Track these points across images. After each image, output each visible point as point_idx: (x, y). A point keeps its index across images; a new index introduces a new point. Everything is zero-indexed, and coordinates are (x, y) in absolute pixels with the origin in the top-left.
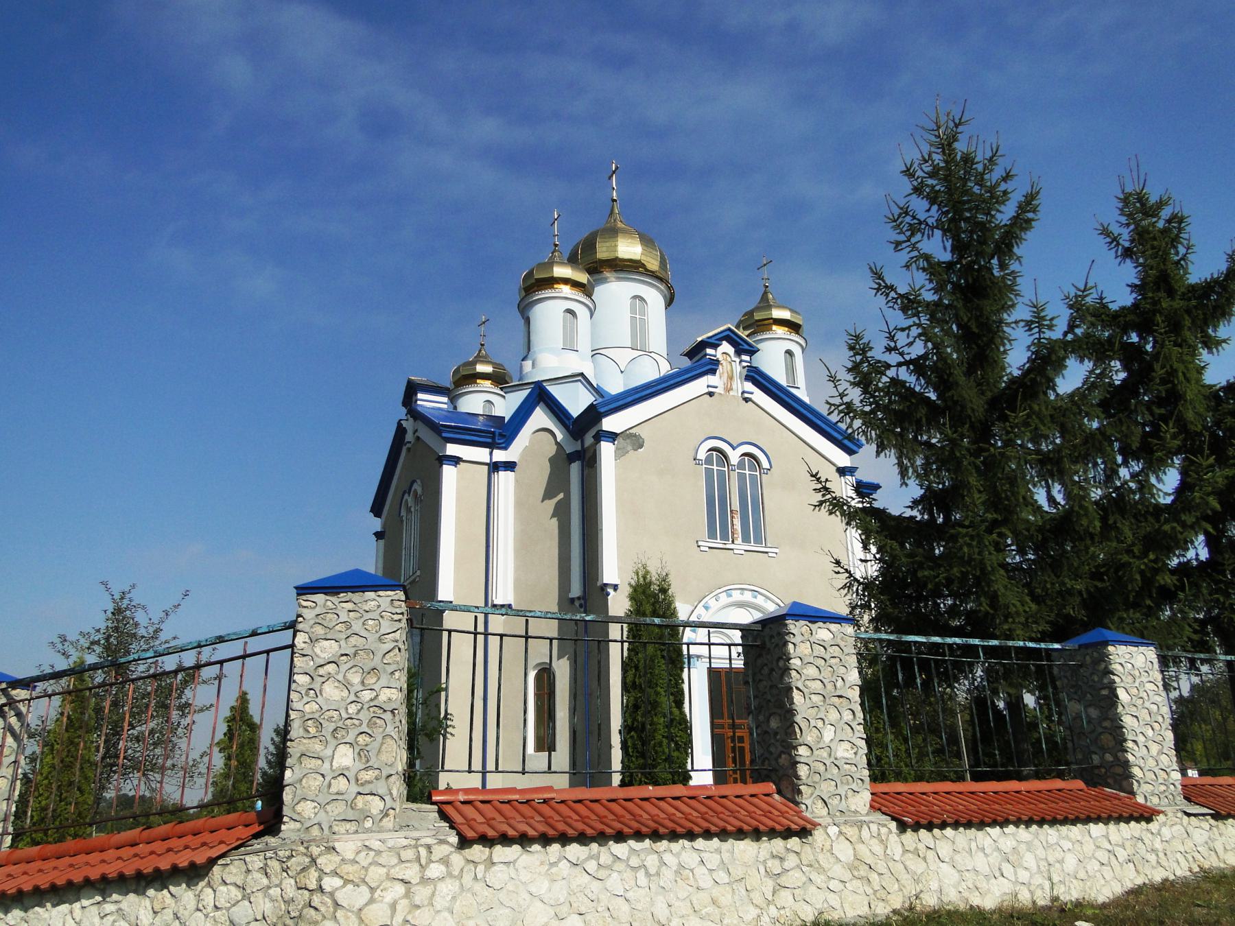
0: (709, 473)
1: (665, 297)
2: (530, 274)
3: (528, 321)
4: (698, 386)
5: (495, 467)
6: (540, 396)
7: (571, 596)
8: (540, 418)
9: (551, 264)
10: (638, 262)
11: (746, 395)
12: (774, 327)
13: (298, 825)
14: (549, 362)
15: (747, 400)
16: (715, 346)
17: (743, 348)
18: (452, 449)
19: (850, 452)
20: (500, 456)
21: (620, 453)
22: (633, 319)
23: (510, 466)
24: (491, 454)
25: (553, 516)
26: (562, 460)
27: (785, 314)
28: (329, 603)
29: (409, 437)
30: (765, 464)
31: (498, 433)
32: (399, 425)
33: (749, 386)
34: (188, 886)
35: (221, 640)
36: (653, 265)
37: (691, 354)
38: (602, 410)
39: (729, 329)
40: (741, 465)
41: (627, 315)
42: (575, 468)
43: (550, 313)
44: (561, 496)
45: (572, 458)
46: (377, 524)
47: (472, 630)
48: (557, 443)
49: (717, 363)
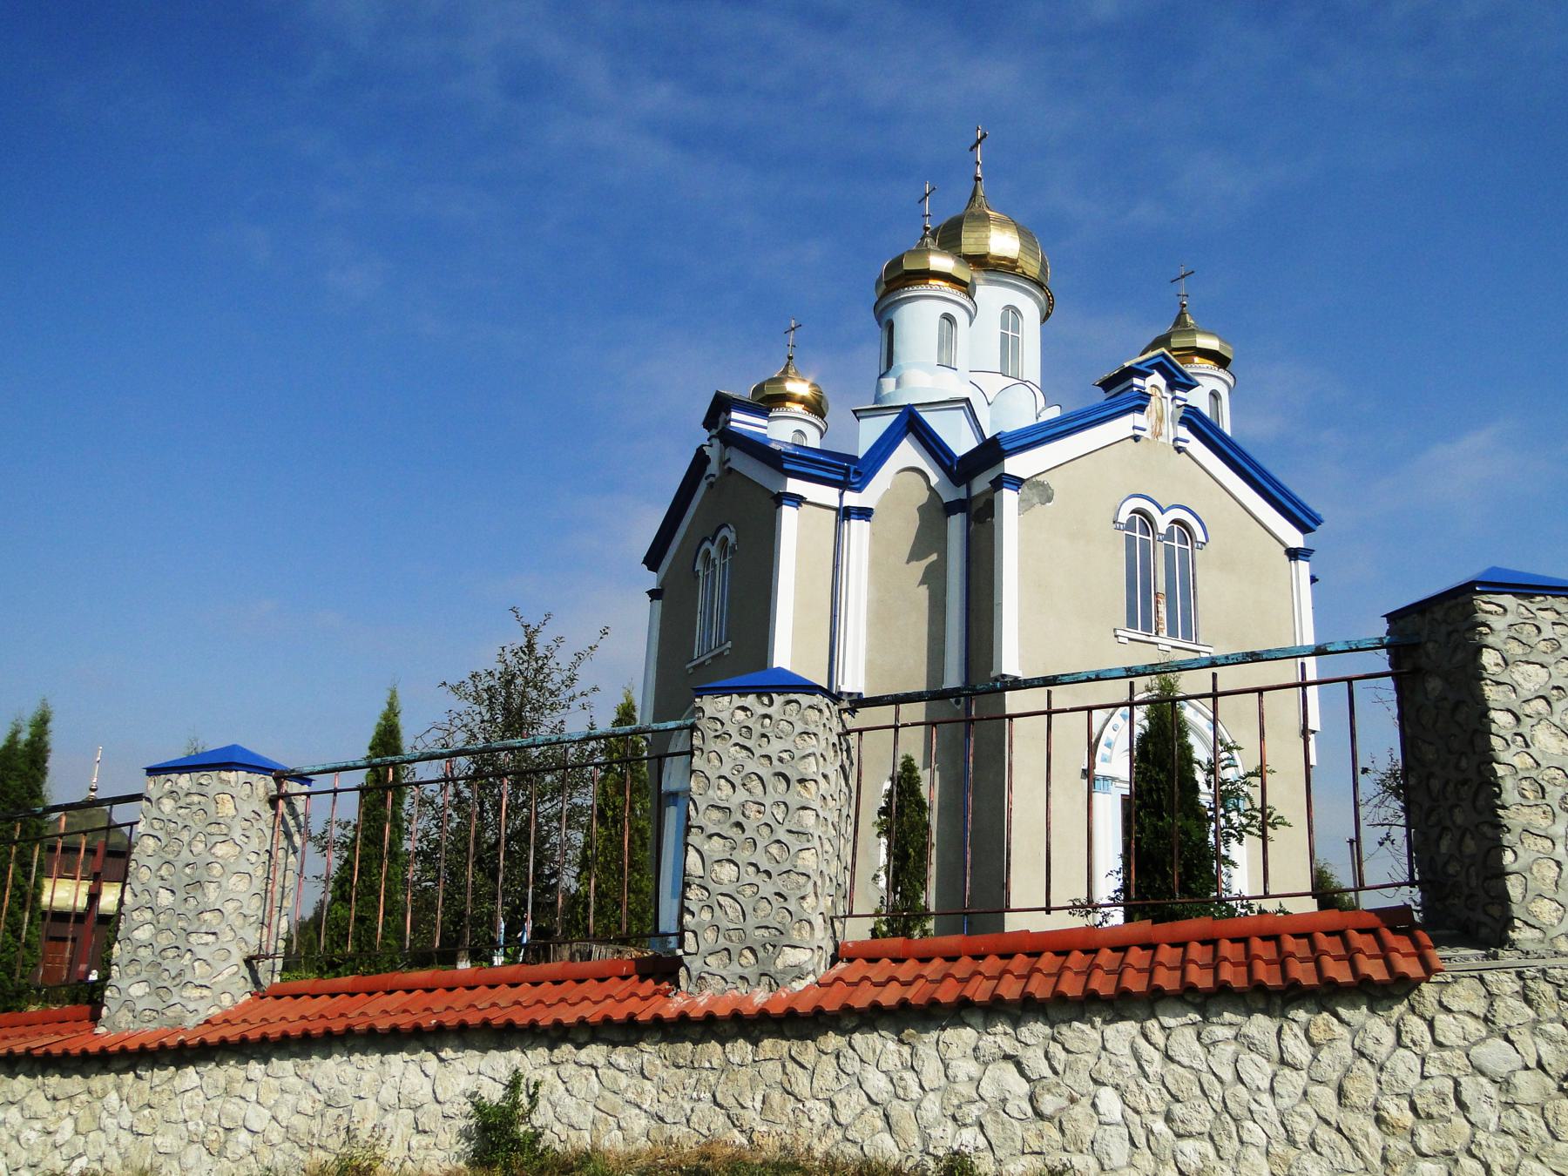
0: (1130, 541)
1: (1041, 311)
2: (897, 263)
3: (890, 327)
4: (1122, 426)
5: (846, 513)
6: (911, 424)
8: (907, 453)
9: (923, 251)
10: (1014, 261)
11: (1180, 444)
12: (1197, 359)
13: (1537, 934)
14: (920, 379)
15: (1179, 450)
16: (1144, 375)
18: (794, 486)
19: (1304, 528)
20: (852, 499)
21: (1025, 506)
22: (1004, 337)
23: (865, 513)
24: (841, 495)
25: (922, 583)
26: (935, 512)
27: (1212, 343)
28: (1522, 609)
29: (713, 468)
30: (1200, 537)
31: (849, 471)
32: (700, 451)
33: (1184, 432)
34: (1372, 1010)
35: (1254, 657)
36: (1033, 269)
37: (1107, 385)
38: (1006, 447)
39: (1163, 355)
40: (1169, 535)
41: (997, 331)
42: (956, 523)
43: (919, 317)
44: (934, 557)
45: (950, 509)
46: (652, 580)
47: (1054, 707)
48: (930, 488)
49: (1146, 397)
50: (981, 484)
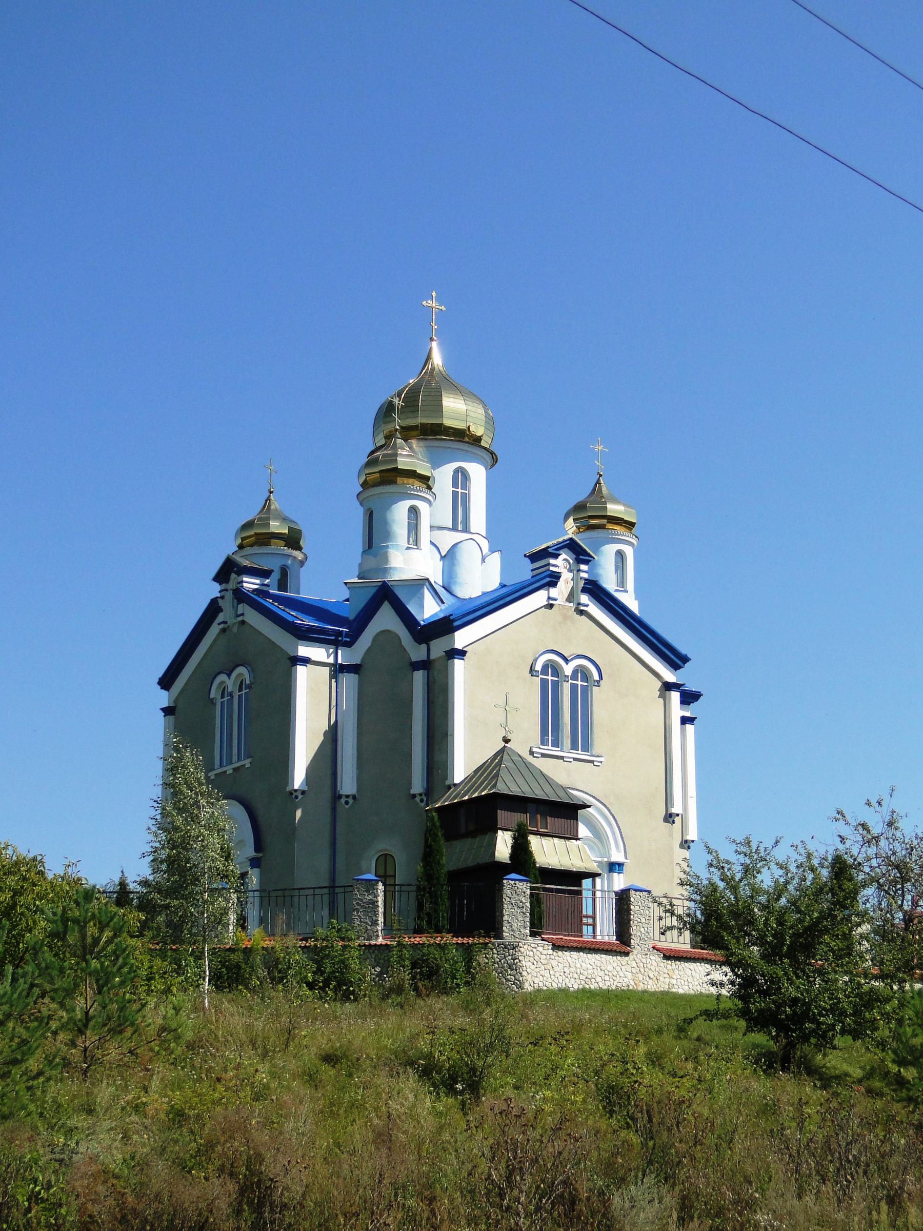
0: (544, 683)
4: (539, 598)
7: (412, 792)
11: (582, 608)
17: (580, 555)
18: (304, 650)
19: (675, 667)
22: (455, 494)
38: (456, 624)
46: (164, 698)
50: (438, 648)
